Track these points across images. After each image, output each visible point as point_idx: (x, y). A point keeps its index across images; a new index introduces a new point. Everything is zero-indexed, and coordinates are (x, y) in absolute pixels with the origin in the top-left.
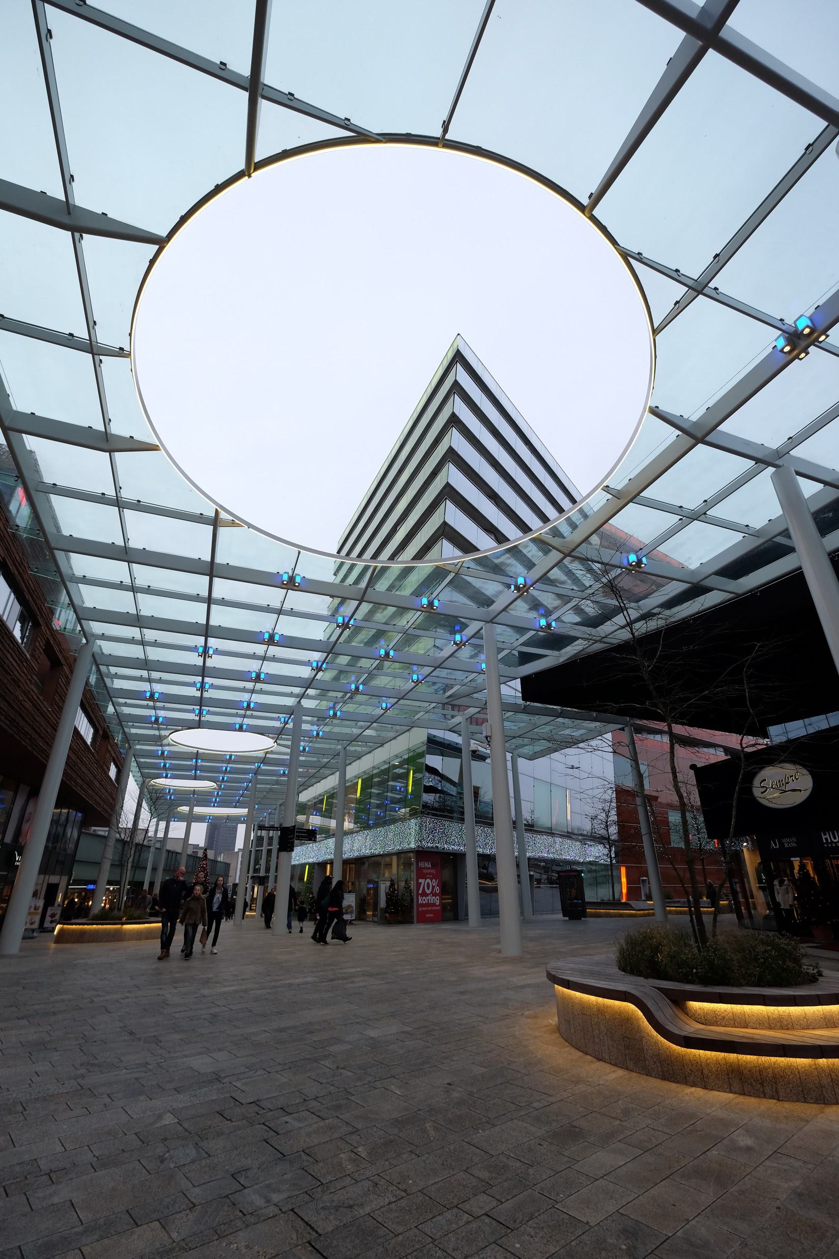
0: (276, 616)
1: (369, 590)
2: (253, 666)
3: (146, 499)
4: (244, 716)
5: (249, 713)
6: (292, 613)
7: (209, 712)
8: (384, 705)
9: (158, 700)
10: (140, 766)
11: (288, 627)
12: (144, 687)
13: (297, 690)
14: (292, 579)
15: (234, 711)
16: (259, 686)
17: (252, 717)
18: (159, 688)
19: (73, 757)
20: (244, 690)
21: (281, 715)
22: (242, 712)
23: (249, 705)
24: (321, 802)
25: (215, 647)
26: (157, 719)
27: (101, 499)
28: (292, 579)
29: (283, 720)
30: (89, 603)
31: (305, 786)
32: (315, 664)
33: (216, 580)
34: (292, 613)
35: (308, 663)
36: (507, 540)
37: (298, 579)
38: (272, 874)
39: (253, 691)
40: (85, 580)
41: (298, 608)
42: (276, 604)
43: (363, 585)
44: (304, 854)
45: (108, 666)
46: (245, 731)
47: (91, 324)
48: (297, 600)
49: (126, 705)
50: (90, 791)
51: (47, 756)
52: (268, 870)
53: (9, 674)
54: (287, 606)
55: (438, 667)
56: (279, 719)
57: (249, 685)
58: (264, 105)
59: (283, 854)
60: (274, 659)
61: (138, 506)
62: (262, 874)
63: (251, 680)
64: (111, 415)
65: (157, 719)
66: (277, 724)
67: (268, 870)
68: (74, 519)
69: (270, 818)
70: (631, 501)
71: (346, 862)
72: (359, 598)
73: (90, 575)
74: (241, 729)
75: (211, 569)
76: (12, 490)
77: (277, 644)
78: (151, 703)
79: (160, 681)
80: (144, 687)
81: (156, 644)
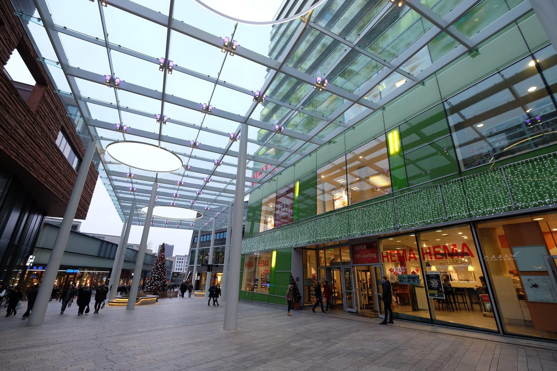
0: (198, 130)
1: (284, 65)
3: (130, 107)
4: (175, 200)
5: (176, 199)
6: (195, 157)
7: (158, 198)
9: (135, 191)
10: (109, 173)
11: (205, 139)
12: (130, 185)
13: (206, 176)
14: (207, 108)
16: (181, 187)
17: (178, 200)
18: (136, 186)
19: (83, 201)
20: (174, 189)
24: (292, 190)
25: (168, 117)
26: (133, 189)
27: (110, 105)
28: (207, 108)
30: (111, 169)
32: (216, 162)
33: (165, 103)
34: (195, 157)
35: (203, 179)
37: (197, 144)
39: (178, 190)
40: (102, 138)
41: (198, 155)
42: (189, 153)
43: (281, 59)
45: (94, 126)
46: (175, 206)
47: (106, 35)
48: (211, 121)
49: (120, 193)
50: (58, 187)
51: (68, 200)
53: (54, 165)
54: (193, 154)
55: (308, 141)
56: (190, 202)
57: (177, 187)
58: (173, 32)
60: (182, 190)
61: (127, 110)
64: (119, 99)
65: (133, 189)
66: (189, 204)
68: (97, 113)
69: (216, 221)
70: (395, 70)
72: (278, 68)
73: (104, 136)
74: (173, 205)
75: (163, 97)
76: (98, 164)
77: (183, 186)
78: (132, 193)
79: (136, 183)
80: (130, 185)
81: (136, 183)
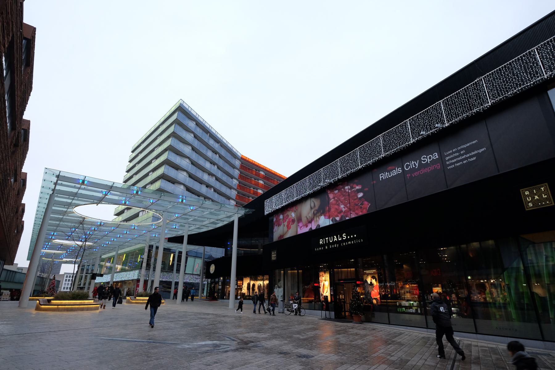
2: (75, 190)
5: (83, 186)
8: (151, 201)
15: (73, 185)
17: (84, 189)
21: (103, 190)
22: (79, 186)
23: (83, 181)
29: (104, 193)
31: (104, 254)
36: (182, 237)
38: (87, 286)
44: (98, 280)
52: (85, 284)
59: (92, 281)
62: (82, 286)
63: (79, 183)
66: (100, 195)
67: (85, 284)
71: (114, 282)
